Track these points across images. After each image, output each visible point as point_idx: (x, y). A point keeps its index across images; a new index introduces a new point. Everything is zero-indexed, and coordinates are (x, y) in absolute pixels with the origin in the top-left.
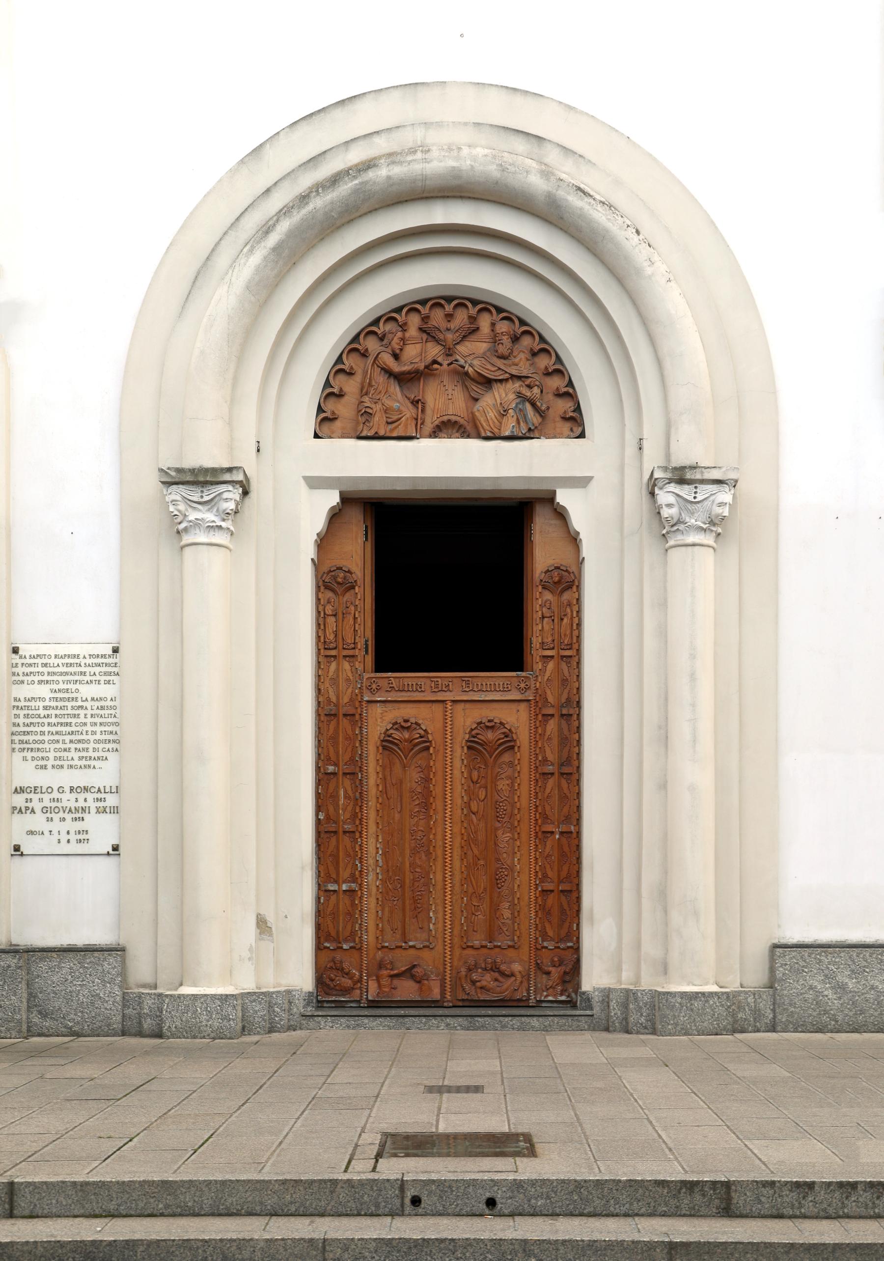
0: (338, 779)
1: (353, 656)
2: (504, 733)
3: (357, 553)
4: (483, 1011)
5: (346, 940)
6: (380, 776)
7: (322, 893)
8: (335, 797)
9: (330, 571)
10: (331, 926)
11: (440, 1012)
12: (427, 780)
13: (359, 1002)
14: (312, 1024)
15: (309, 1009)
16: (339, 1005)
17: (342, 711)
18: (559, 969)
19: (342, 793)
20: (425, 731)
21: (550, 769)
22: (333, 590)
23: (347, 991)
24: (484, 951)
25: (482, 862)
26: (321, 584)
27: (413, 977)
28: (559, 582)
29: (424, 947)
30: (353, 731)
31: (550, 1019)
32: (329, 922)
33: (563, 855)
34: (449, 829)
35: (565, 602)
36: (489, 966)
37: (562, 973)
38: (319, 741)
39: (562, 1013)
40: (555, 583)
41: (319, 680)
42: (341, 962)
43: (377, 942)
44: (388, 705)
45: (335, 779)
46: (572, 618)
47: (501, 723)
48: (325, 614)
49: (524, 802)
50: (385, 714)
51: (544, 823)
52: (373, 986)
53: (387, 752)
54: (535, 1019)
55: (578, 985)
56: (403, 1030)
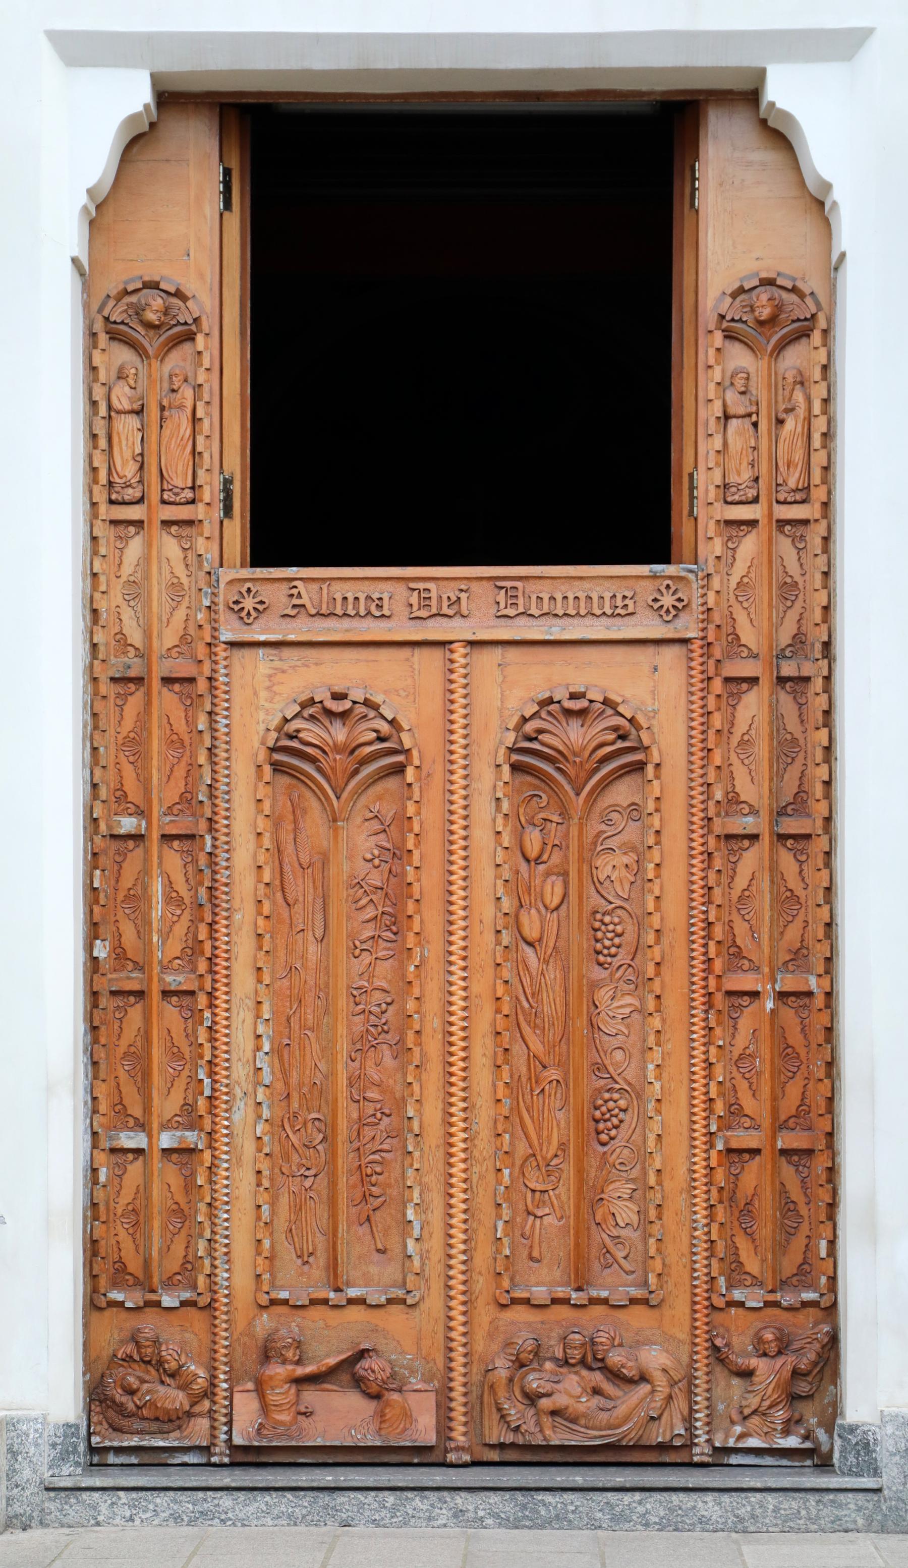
0: (147, 851)
1: (190, 523)
2: (615, 729)
3: (199, 241)
4: (559, 1477)
5: (170, 1283)
6: (267, 842)
7: (101, 1157)
8: (137, 900)
9: (126, 293)
10: (128, 1245)
11: (438, 1477)
12: (399, 854)
13: (206, 1450)
14: (74, 1508)
15: (66, 1470)
16: (153, 1459)
17: (161, 668)
18: (780, 1361)
19: (158, 888)
20: (393, 722)
21: (747, 824)
22: (133, 345)
23: (173, 1420)
24: (563, 1312)
25: (553, 1074)
26: (99, 326)
27: (358, 1382)
28: (772, 321)
29: (390, 1301)
30: (190, 722)
31: (755, 1497)
32: (123, 1235)
33: (785, 1053)
34: (460, 979)
35: (790, 376)
36: (576, 1354)
37: (786, 1373)
38: (95, 749)
39: (787, 1481)
40: (761, 323)
41: (95, 587)
42: (156, 1342)
43: (258, 1289)
44: (287, 652)
45: (139, 851)
46: (809, 418)
47: (606, 702)
48: (110, 407)
49: (674, 912)
50: (280, 677)
51: (730, 968)
52: (246, 1409)
53: (284, 780)
54: (709, 1497)
55: (835, 1409)
56: (332, 1528)
